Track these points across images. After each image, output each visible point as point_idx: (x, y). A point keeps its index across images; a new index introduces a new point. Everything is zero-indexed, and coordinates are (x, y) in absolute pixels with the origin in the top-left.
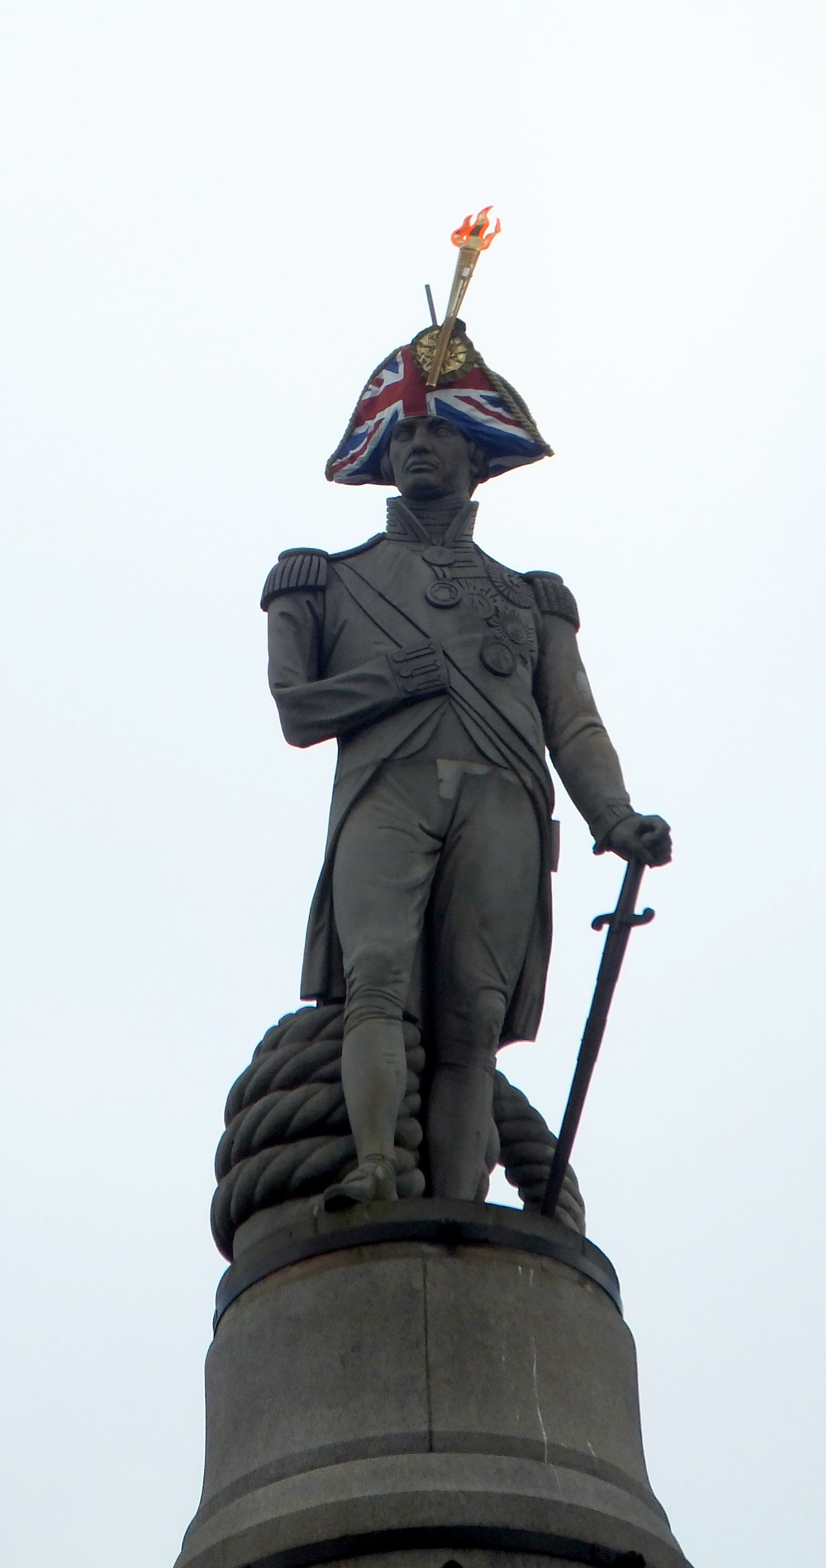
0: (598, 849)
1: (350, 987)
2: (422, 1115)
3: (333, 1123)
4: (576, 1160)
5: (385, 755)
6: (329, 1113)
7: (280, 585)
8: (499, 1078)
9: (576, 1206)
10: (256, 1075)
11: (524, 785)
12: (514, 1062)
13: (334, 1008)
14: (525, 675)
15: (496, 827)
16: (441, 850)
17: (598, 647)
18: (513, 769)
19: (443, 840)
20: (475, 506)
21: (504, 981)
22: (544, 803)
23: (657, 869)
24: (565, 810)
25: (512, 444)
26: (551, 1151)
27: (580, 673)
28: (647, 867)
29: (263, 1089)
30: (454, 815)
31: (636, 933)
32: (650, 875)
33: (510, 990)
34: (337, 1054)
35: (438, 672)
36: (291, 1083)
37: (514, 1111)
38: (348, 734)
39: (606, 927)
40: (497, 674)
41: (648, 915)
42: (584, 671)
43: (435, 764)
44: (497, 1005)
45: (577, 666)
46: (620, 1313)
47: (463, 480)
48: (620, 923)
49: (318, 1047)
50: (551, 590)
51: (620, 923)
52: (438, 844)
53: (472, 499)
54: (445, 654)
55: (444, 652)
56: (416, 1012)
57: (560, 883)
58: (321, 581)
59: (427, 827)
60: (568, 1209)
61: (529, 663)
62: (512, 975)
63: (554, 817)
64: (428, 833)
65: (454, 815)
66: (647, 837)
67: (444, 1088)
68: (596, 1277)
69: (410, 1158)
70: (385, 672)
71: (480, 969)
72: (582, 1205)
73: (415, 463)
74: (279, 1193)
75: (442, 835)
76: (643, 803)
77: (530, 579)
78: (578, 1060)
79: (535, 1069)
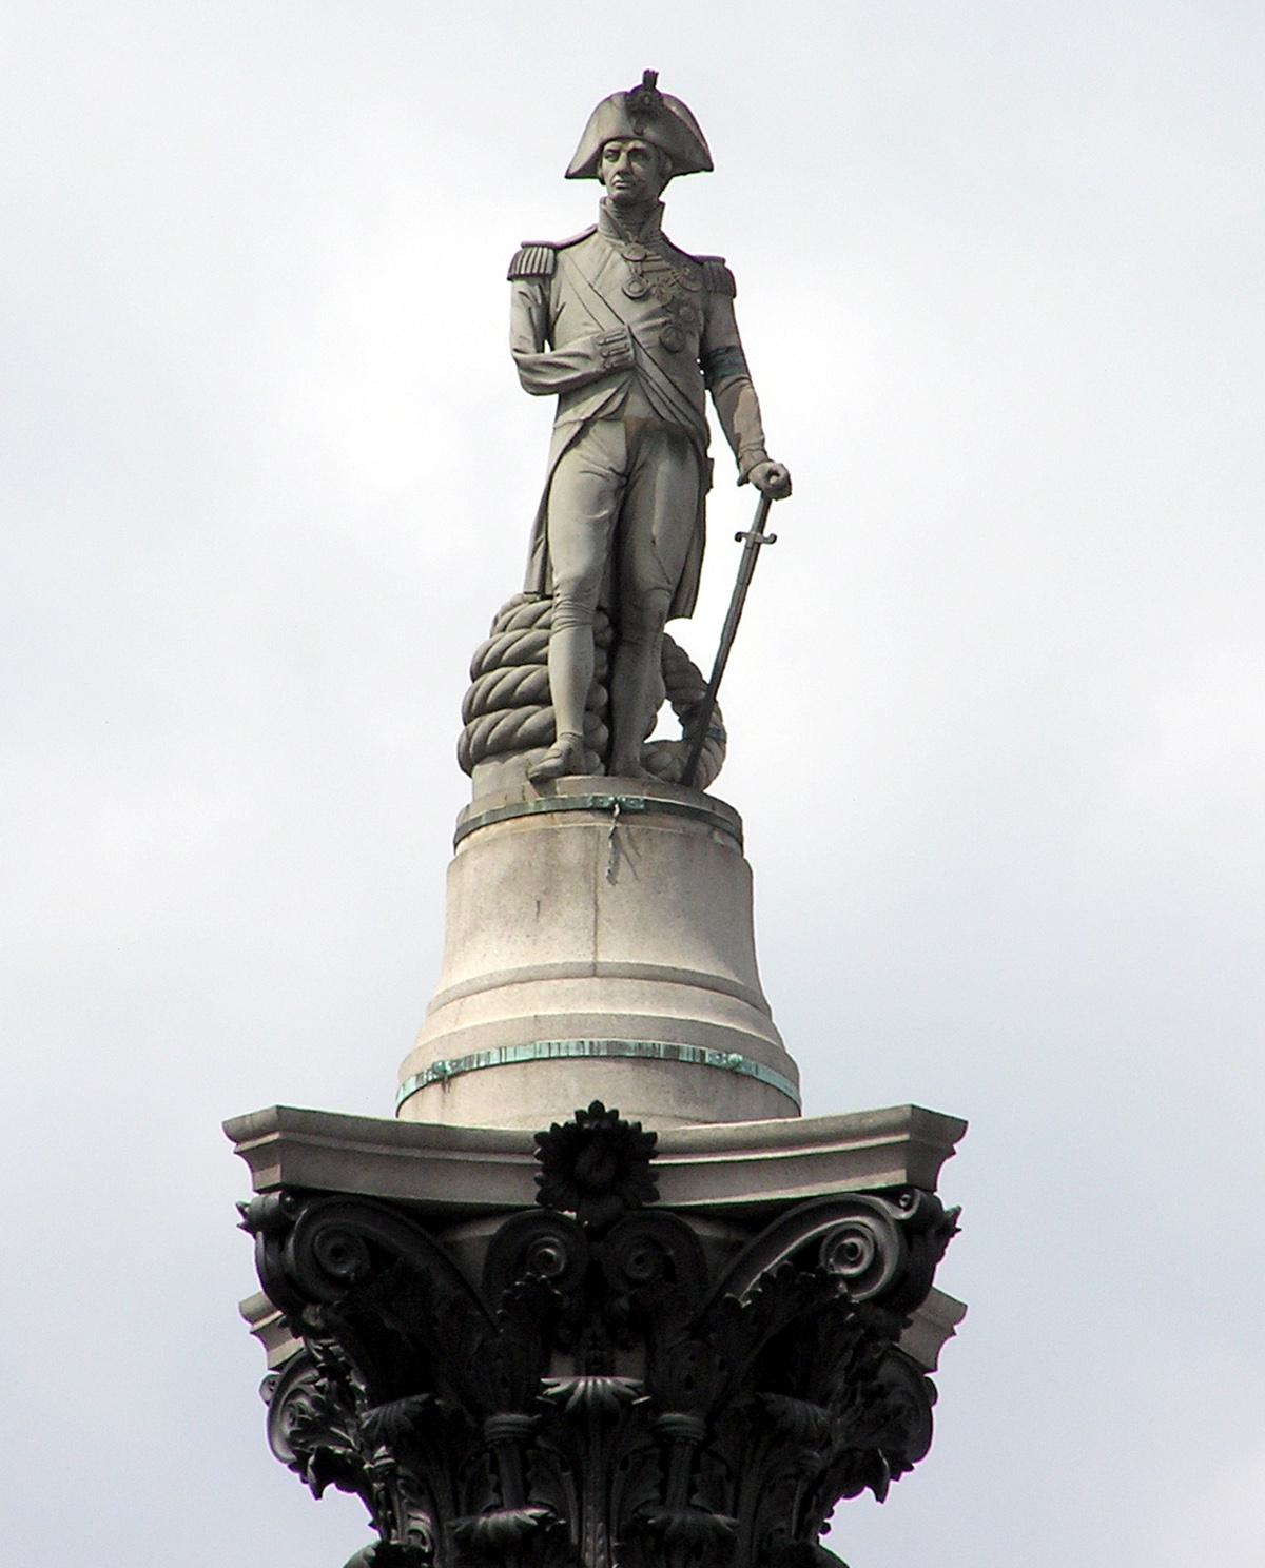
2: (607, 682)
3: (540, 697)
4: (722, 696)
5: (588, 415)
6: (540, 691)
8: (669, 640)
10: (492, 650)
12: (675, 628)
13: (547, 602)
20: (662, 205)
21: (669, 582)
23: (781, 501)
29: (495, 664)
32: (776, 506)
33: (673, 588)
34: (547, 643)
35: (627, 354)
36: (516, 662)
37: (677, 664)
38: (568, 394)
44: (663, 600)
47: (652, 191)
48: (754, 542)
49: (536, 634)
50: (715, 274)
51: (754, 542)
52: (624, 480)
53: (662, 199)
58: (549, 271)
66: (773, 480)
67: (625, 656)
70: (589, 351)
71: (649, 569)
72: (724, 756)
73: (618, 181)
74: (506, 746)
75: (627, 474)
76: (780, 450)
77: (698, 262)
79: (695, 637)
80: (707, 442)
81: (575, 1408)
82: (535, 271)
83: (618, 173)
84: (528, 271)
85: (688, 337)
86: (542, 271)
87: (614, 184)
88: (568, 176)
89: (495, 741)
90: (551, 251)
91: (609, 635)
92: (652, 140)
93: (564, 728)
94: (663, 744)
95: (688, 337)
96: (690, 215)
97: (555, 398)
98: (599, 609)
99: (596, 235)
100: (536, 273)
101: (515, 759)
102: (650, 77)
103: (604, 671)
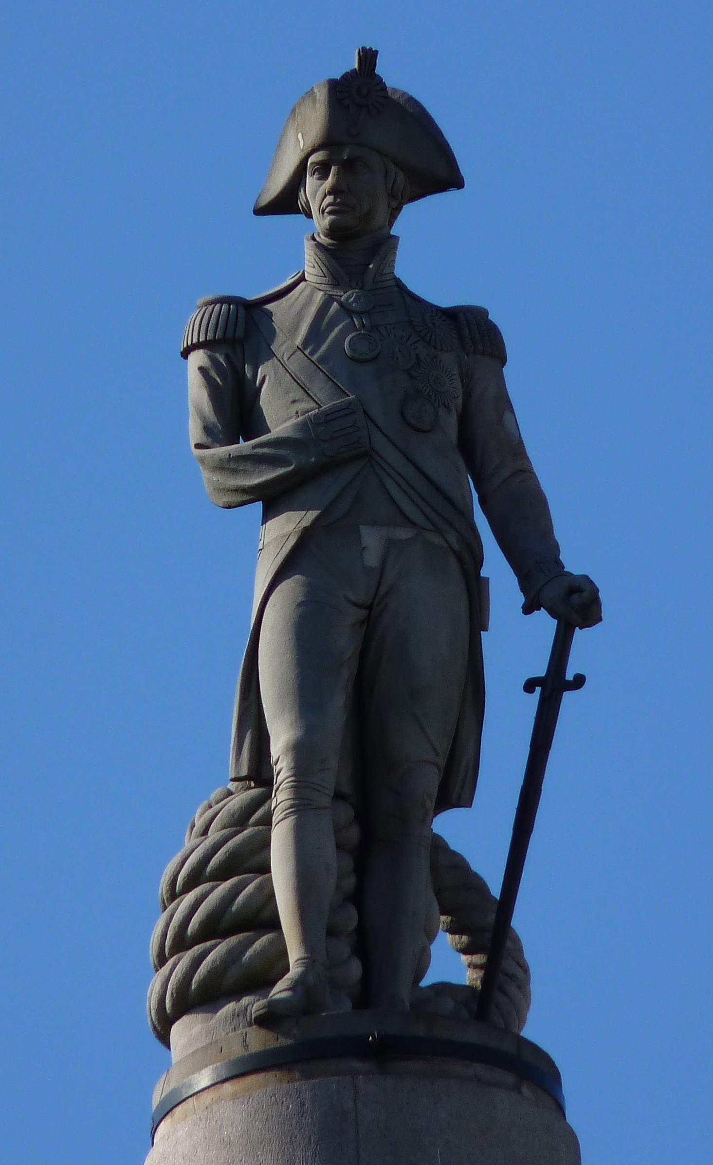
0: (528, 609)
1: (278, 775)
2: (356, 898)
4: (519, 922)
7: (199, 339)
8: (438, 845)
9: (519, 972)
11: (450, 546)
12: (449, 826)
14: (451, 424)
15: (425, 598)
16: (369, 618)
17: (524, 381)
18: (438, 530)
19: (370, 608)
20: (396, 238)
22: (471, 558)
24: (496, 567)
25: (434, 170)
26: (492, 918)
27: (507, 415)
28: (577, 628)
30: (379, 583)
31: (569, 698)
33: (442, 762)
37: (453, 878)
39: (538, 689)
40: (418, 430)
41: (579, 681)
42: (513, 412)
43: (358, 532)
44: (429, 781)
45: (504, 404)
46: (560, 1109)
47: (380, 217)
48: (553, 686)
51: (553, 686)
54: (365, 412)
55: (364, 411)
56: (347, 789)
57: (491, 642)
59: (353, 599)
60: (512, 977)
61: (454, 412)
62: (444, 746)
63: (483, 573)
64: (356, 605)
65: (379, 583)
66: (576, 599)
68: (537, 1074)
69: (344, 948)
76: (574, 561)
77: (453, 315)
78: (514, 830)
79: (474, 834)
80: (479, 561)
81: (331, 238)
82: (195, 341)
83: (330, 193)
84: (202, 339)
85: (442, 412)
86: (230, 334)
87: (323, 211)
88: (260, 211)
89: (203, 983)
90: (242, 311)
91: (354, 834)
92: (381, 146)
93: (295, 953)
94: (443, 989)
95: (442, 412)
96: (436, 252)
97: (259, 506)
98: (338, 796)
99: (302, 285)
100: (239, 333)
101: (230, 1007)
102: (368, 57)
103: (350, 882)
